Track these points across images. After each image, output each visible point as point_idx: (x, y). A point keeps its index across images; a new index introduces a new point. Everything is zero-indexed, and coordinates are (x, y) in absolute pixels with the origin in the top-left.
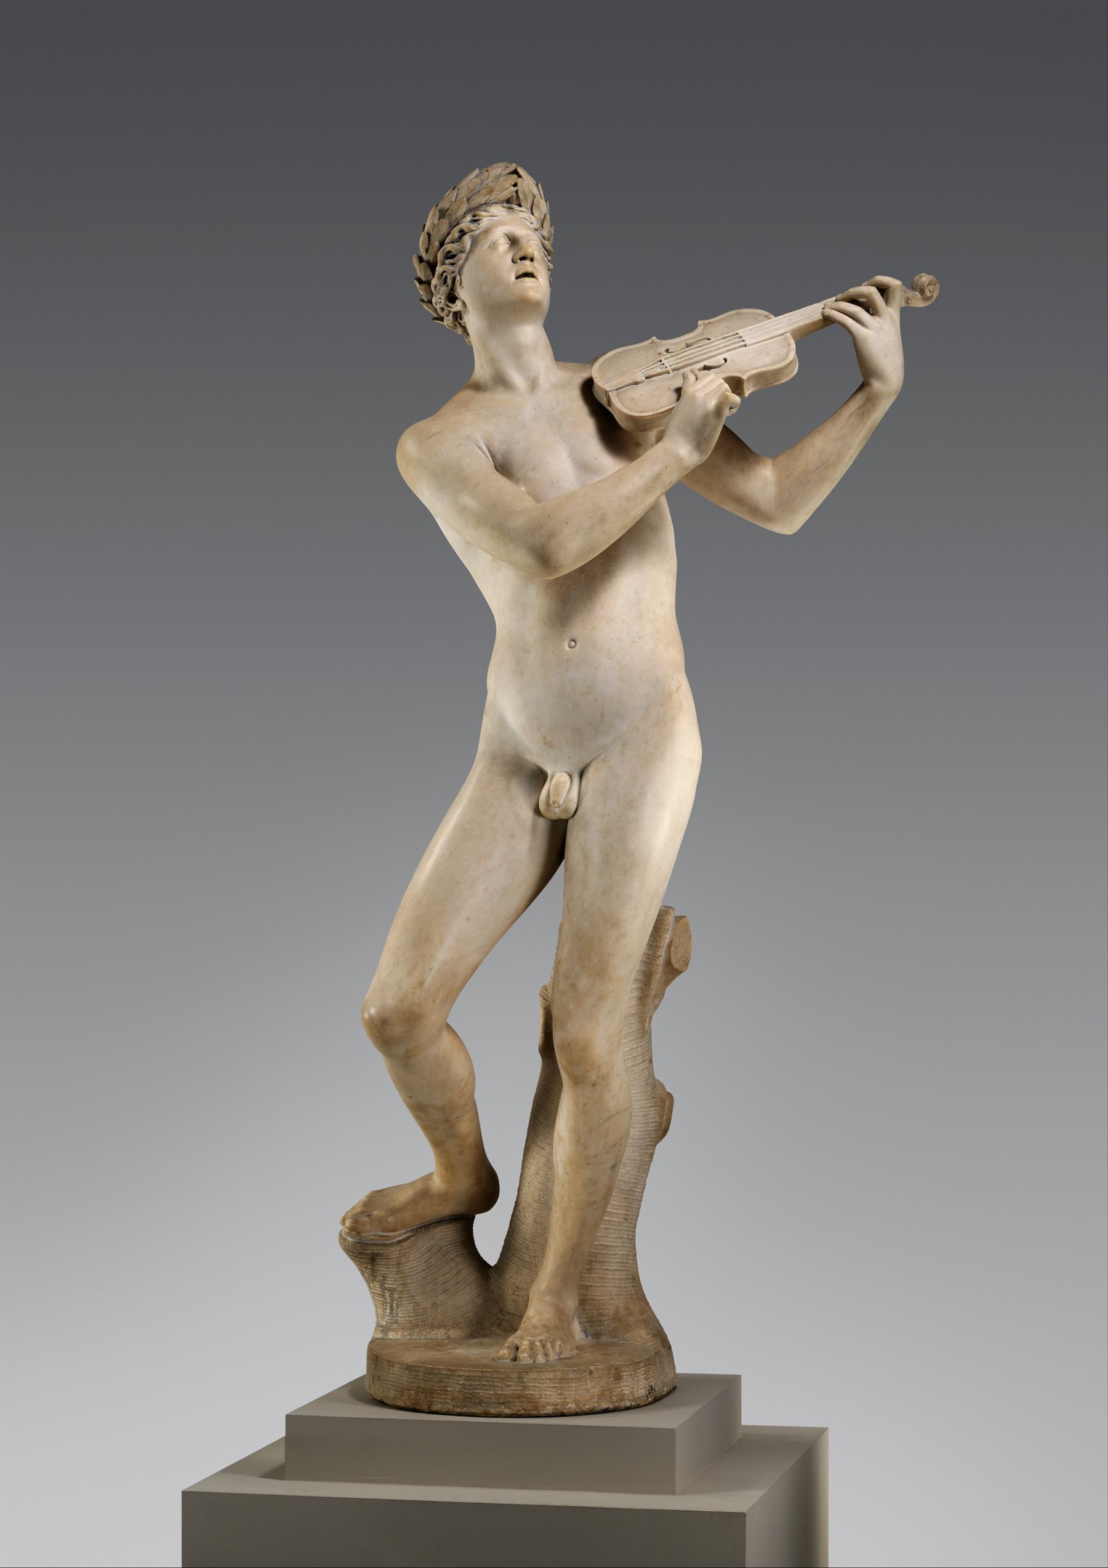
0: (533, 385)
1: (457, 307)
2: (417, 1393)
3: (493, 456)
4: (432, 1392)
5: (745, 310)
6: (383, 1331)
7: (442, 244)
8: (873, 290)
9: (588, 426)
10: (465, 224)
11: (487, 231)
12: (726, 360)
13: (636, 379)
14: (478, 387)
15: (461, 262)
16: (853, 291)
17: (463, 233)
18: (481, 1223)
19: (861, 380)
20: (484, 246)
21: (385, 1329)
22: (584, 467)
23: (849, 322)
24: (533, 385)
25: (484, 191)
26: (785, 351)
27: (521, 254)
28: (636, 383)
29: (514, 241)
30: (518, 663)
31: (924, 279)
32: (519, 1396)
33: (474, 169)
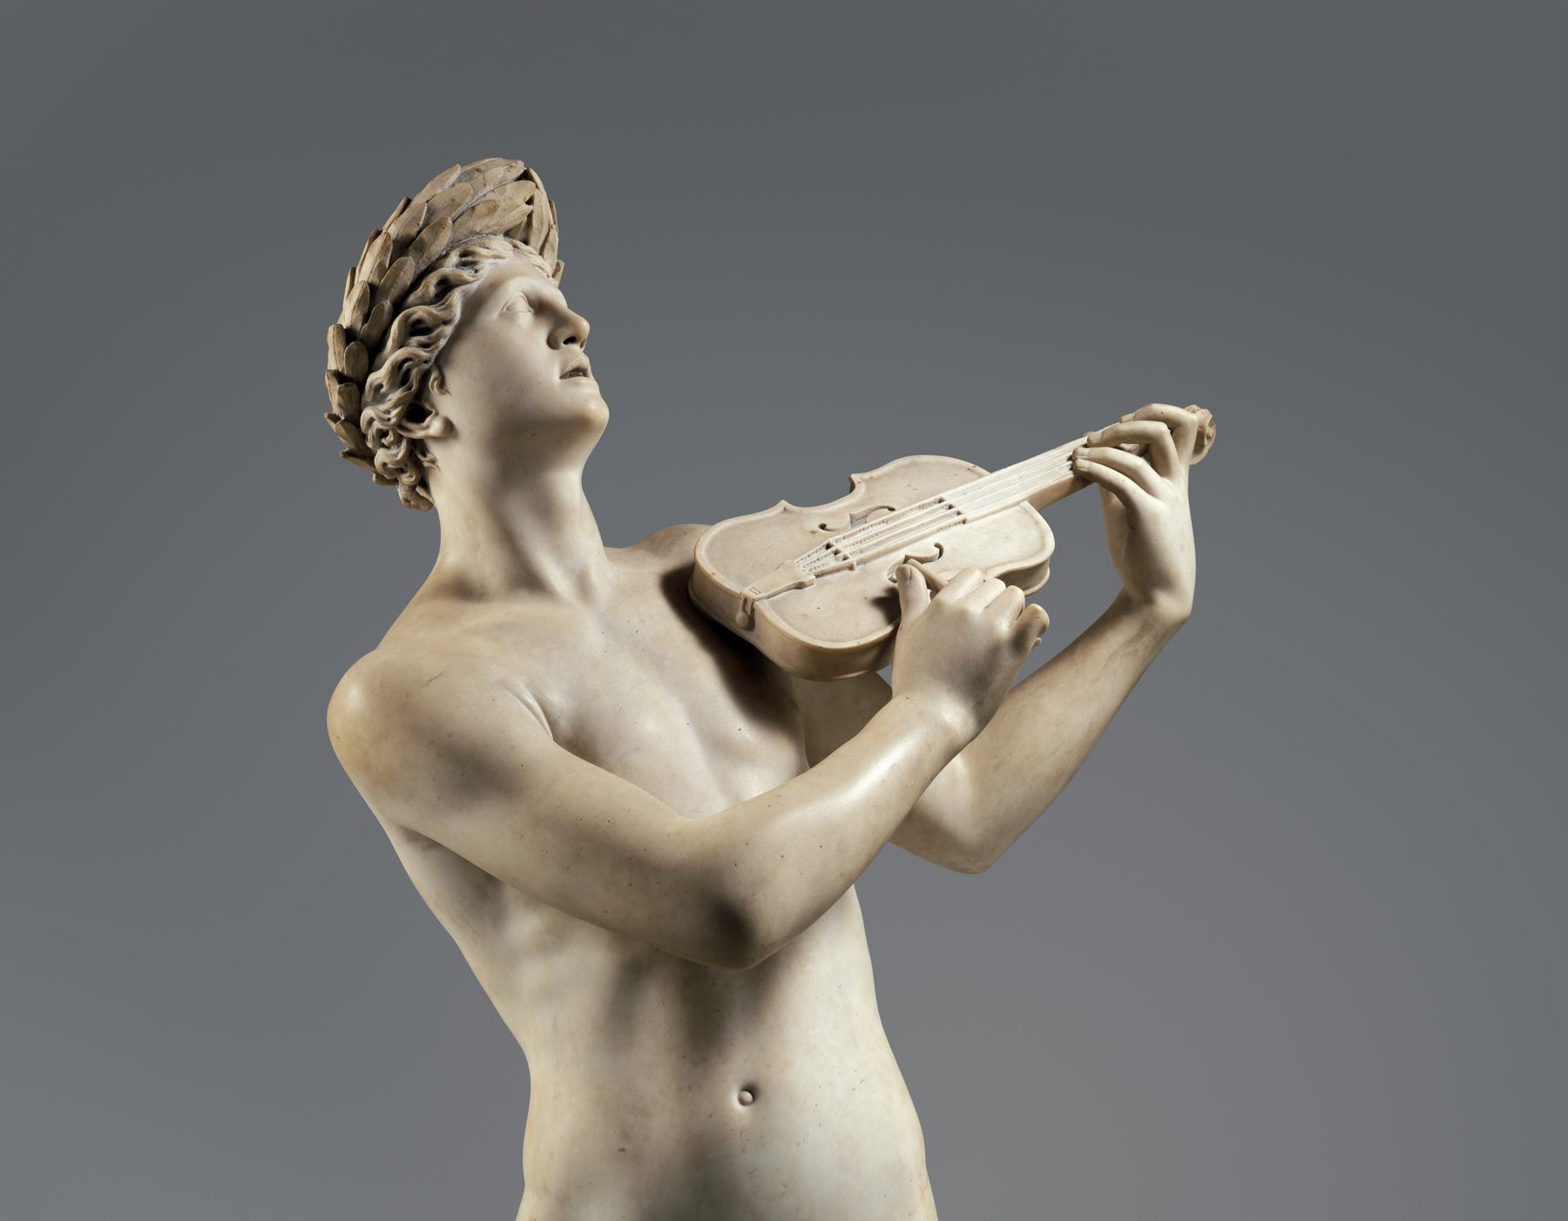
0: (583, 585)
3: (553, 724)
7: (399, 305)
10: (450, 267)
11: (493, 287)
13: (803, 575)
14: (464, 590)
16: (1129, 424)
17: (446, 286)
20: (491, 316)
22: (721, 749)
26: (1034, 535)
28: (800, 586)
29: (540, 308)
33: (450, 165)
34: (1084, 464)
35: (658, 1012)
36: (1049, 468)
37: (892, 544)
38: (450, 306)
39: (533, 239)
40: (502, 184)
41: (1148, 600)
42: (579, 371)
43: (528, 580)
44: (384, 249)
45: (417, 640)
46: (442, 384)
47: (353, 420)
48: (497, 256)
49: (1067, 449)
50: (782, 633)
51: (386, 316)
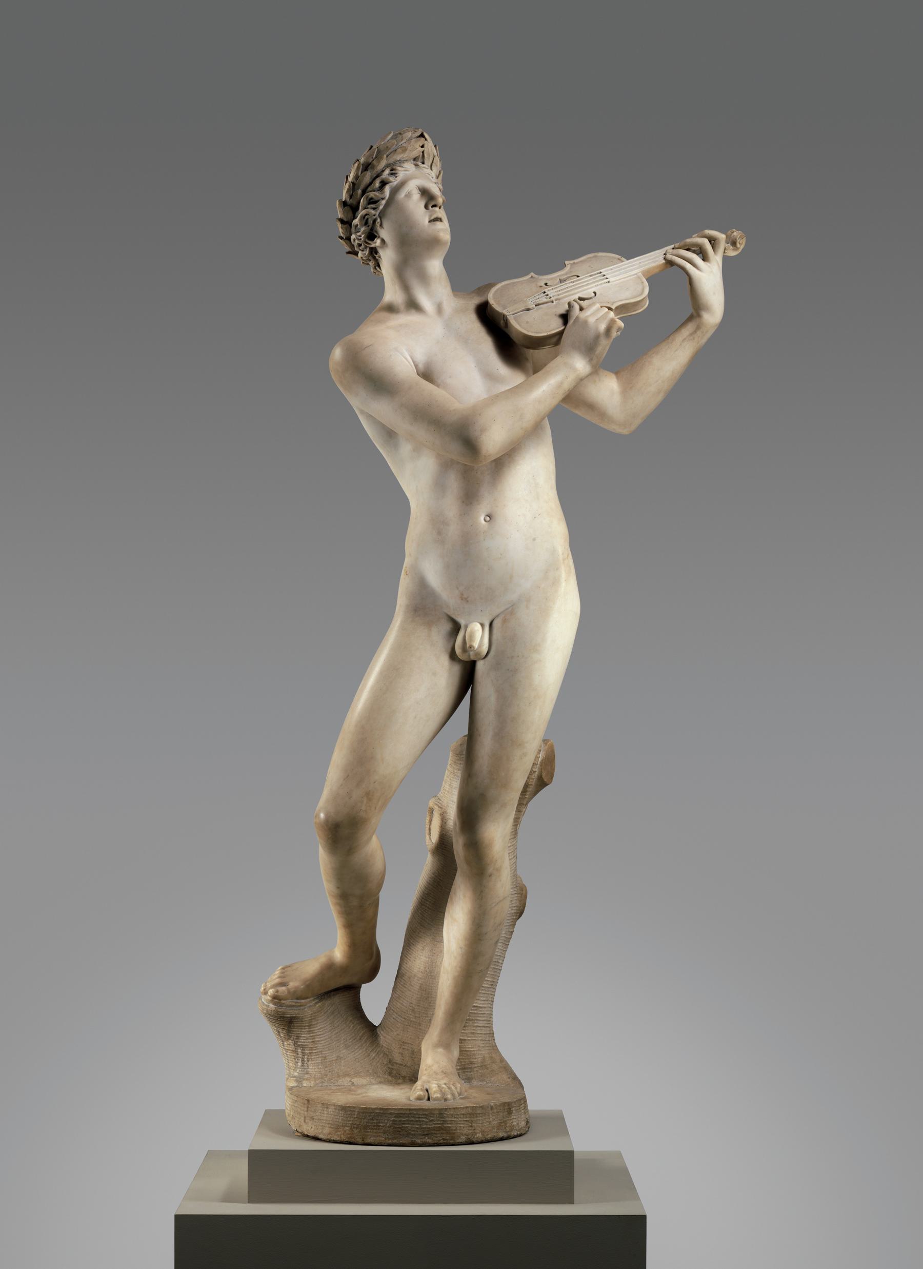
2: (352, 1129)
5: (600, 254)
6: (297, 1081)
8: (706, 241)
9: (486, 344)
11: (402, 184)
12: (595, 293)
14: (391, 309)
17: (384, 183)
18: (366, 991)
19: (690, 311)
20: (402, 195)
21: (299, 1080)
22: (490, 376)
24: (439, 310)
26: (640, 288)
27: (433, 203)
28: (528, 310)
29: (425, 193)
30: (439, 533)
31: (735, 234)
32: (440, 1129)
34: (669, 257)
35: (453, 482)
36: (654, 259)
39: (426, 162)
40: (410, 139)
41: (699, 316)
43: (413, 305)
44: (358, 168)
46: (381, 225)
47: (348, 239)
48: (407, 170)
49: (663, 251)
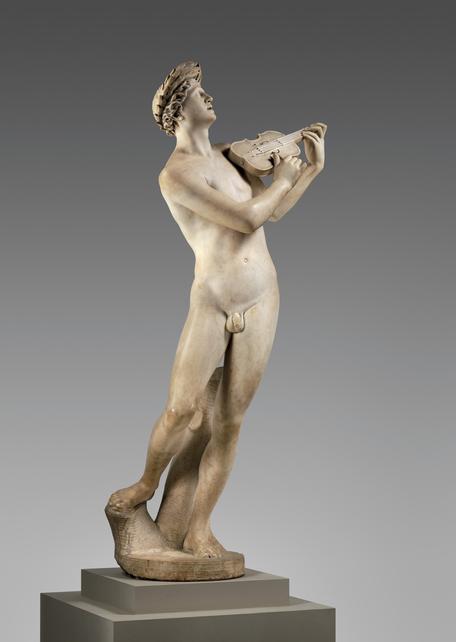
1: (176, 119)
2: (178, 574)
3: (207, 182)
4: (186, 572)
5: (271, 131)
8: (321, 128)
13: (255, 155)
15: (183, 100)
16: (313, 127)
20: (193, 95)
23: (314, 140)
25: (191, 72)
27: (209, 100)
28: (253, 157)
29: (202, 95)
32: (223, 571)
34: (305, 135)
37: (268, 150)
38: (185, 93)
42: (210, 108)
45: (174, 163)
49: (301, 131)
50: (251, 166)
51: (171, 94)
